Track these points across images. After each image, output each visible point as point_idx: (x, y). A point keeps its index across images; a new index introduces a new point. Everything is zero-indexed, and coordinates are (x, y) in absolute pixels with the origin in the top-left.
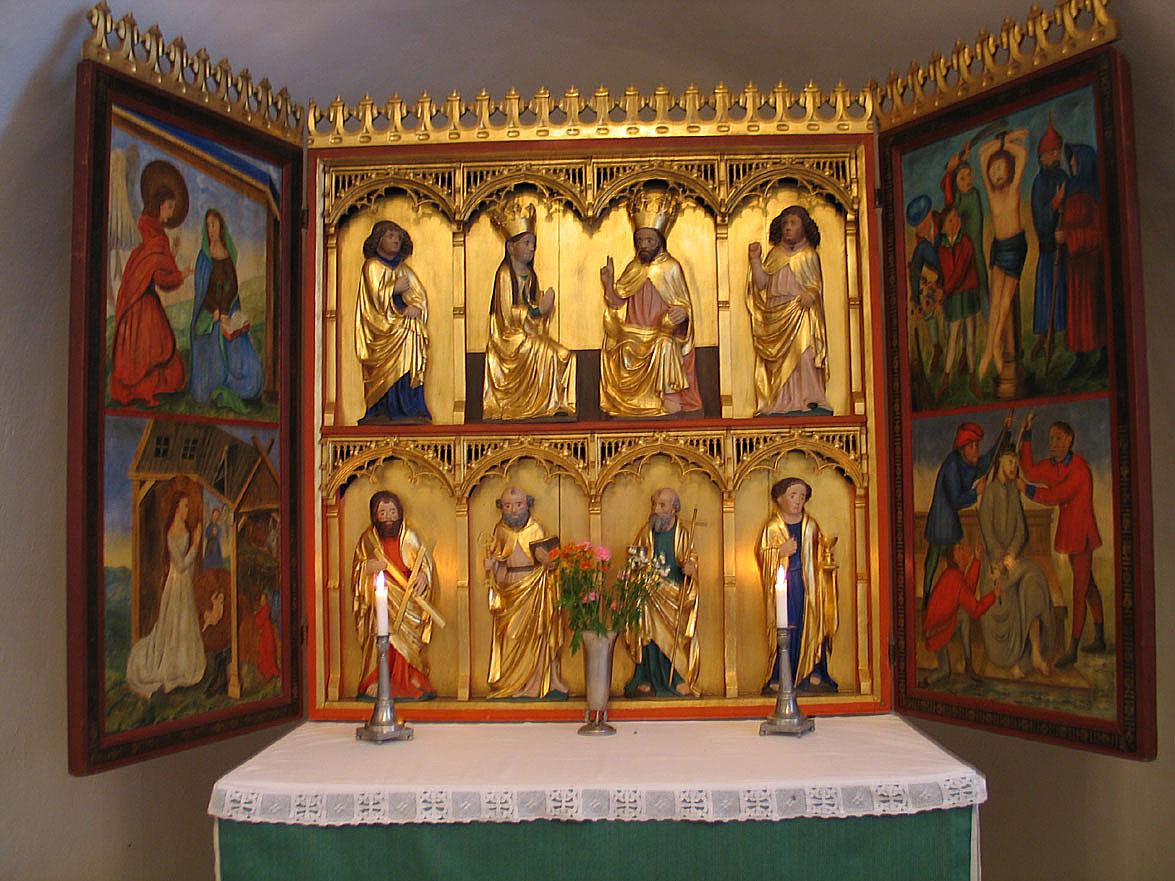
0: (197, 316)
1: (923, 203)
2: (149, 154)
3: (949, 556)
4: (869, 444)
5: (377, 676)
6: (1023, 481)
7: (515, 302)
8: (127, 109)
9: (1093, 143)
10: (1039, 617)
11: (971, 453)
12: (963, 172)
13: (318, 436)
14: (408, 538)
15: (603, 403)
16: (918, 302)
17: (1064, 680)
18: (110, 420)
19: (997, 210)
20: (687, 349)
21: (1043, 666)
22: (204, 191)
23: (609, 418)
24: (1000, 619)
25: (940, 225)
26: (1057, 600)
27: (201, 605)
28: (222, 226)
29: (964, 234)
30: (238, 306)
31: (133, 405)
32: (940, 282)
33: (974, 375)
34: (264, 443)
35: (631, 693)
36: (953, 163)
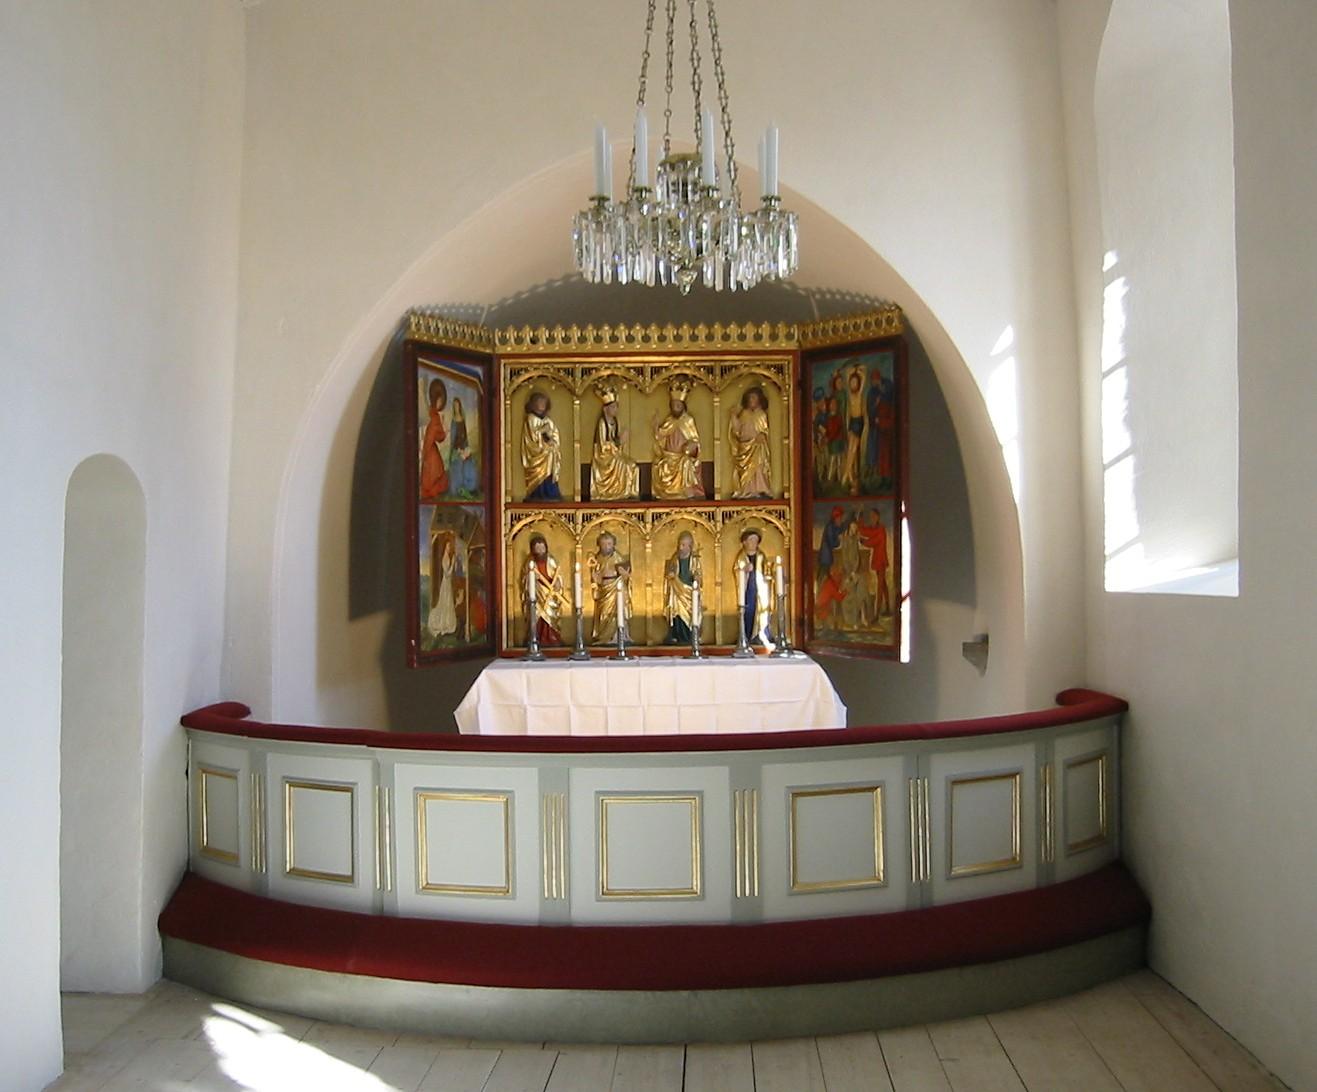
0: (452, 452)
1: (821, 392)
2: (432, 377)
3: (828, 573)
4: (791, 513)
5: (788, 490)
6: (859, 536)
7: (607, 439)
8: (425, 358)
9: (892, 378)
10: (864, 601)
11: (838, 522)
12: (839, 380)
13: (503, 508)
14: (551, 562)
15: (653, 492)
16: (817, 443)
17: (873, 629)
18: (421, 507)
19: (853, 403)
20: (697, 464)
21: (866, 624)
22: (453, 389)
23: (656, 500)
24: (850, 602)
25: (828, 406)
26: (872, 593)
27: (455, 595)
28: (460, 405)
29: (838, 412)
30: (467, 445)
31: (429, 500)
32: (828, 434)
33: (840, 483)
34: (478, 513)
35: (667, 643)
36: (835, 374)
